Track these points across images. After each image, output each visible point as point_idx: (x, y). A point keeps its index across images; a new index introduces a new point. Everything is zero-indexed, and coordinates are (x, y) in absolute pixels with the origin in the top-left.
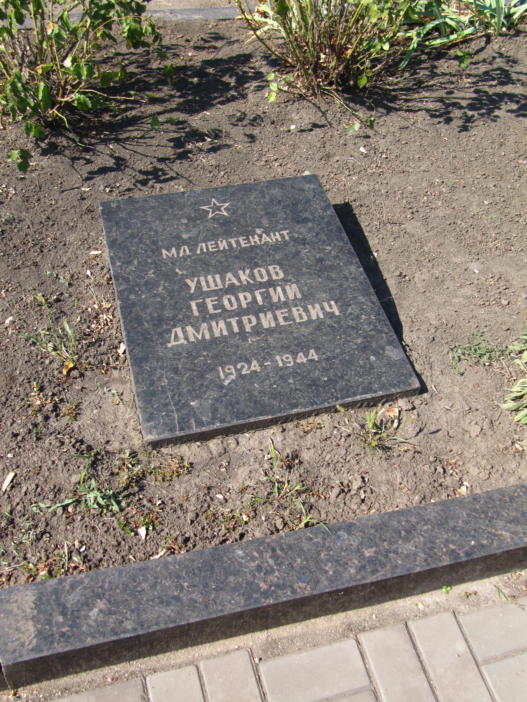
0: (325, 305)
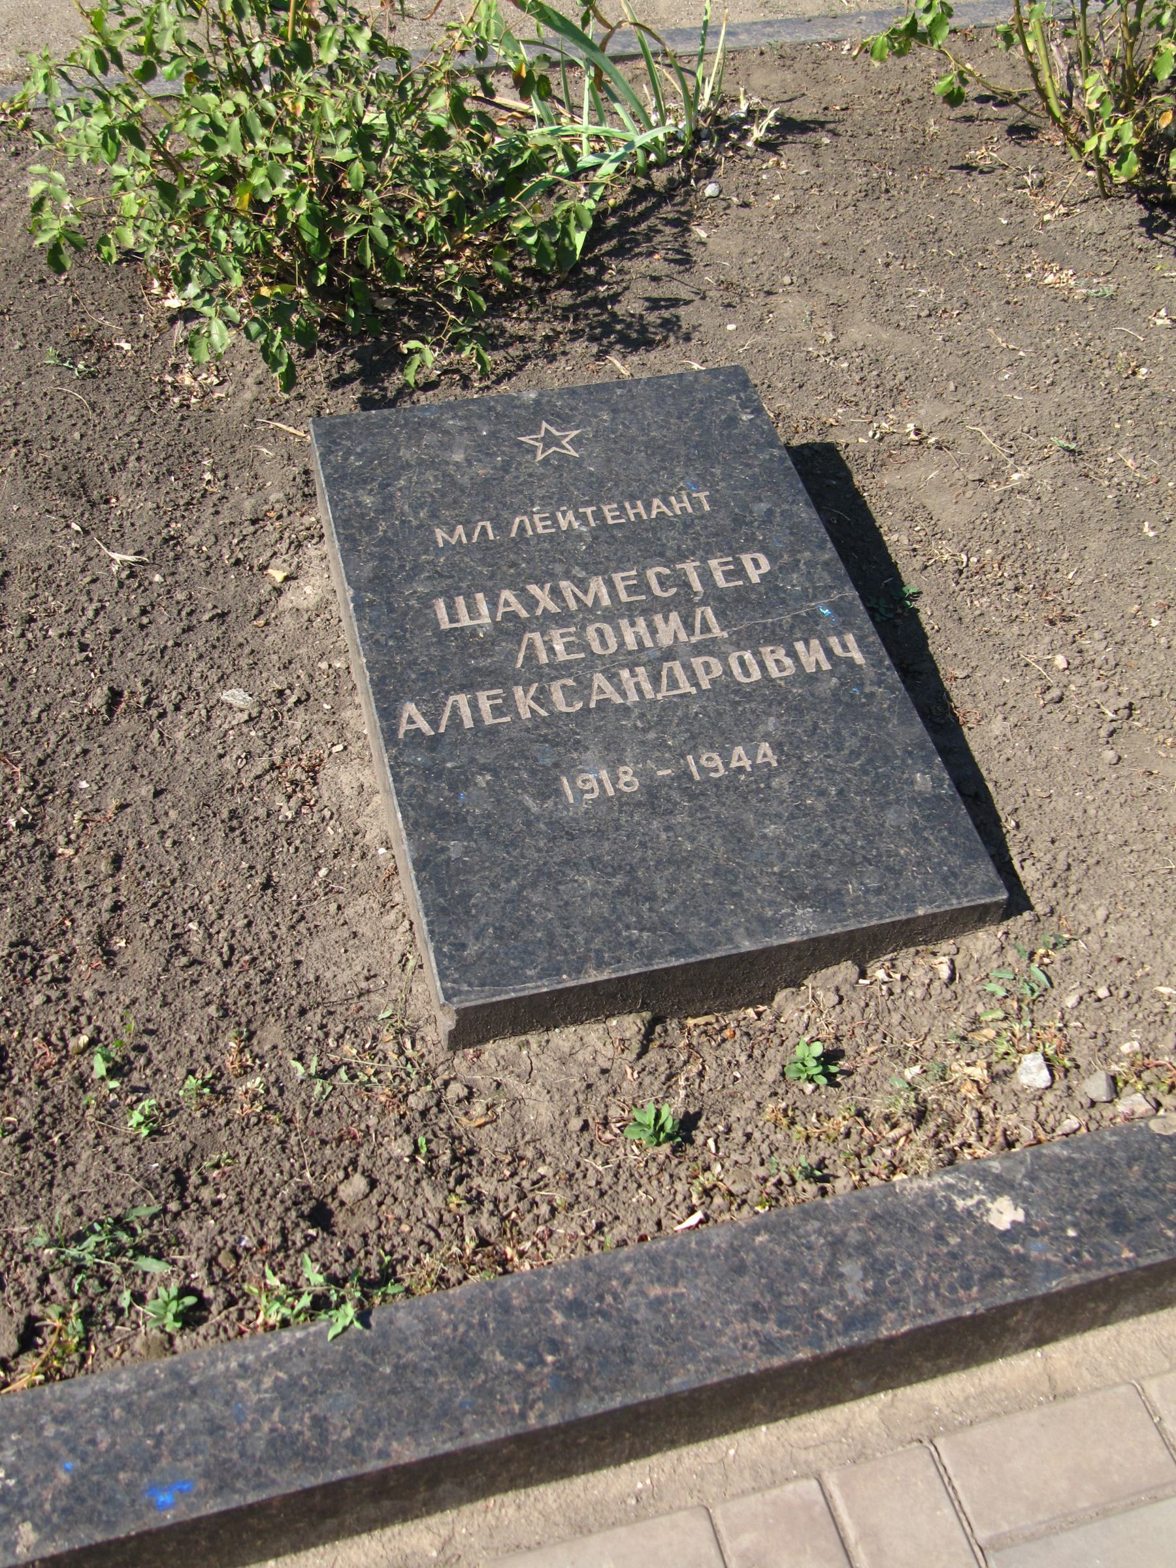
0: (834, 641)
